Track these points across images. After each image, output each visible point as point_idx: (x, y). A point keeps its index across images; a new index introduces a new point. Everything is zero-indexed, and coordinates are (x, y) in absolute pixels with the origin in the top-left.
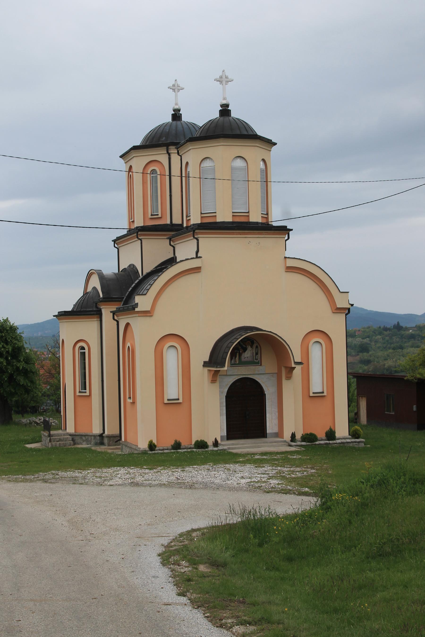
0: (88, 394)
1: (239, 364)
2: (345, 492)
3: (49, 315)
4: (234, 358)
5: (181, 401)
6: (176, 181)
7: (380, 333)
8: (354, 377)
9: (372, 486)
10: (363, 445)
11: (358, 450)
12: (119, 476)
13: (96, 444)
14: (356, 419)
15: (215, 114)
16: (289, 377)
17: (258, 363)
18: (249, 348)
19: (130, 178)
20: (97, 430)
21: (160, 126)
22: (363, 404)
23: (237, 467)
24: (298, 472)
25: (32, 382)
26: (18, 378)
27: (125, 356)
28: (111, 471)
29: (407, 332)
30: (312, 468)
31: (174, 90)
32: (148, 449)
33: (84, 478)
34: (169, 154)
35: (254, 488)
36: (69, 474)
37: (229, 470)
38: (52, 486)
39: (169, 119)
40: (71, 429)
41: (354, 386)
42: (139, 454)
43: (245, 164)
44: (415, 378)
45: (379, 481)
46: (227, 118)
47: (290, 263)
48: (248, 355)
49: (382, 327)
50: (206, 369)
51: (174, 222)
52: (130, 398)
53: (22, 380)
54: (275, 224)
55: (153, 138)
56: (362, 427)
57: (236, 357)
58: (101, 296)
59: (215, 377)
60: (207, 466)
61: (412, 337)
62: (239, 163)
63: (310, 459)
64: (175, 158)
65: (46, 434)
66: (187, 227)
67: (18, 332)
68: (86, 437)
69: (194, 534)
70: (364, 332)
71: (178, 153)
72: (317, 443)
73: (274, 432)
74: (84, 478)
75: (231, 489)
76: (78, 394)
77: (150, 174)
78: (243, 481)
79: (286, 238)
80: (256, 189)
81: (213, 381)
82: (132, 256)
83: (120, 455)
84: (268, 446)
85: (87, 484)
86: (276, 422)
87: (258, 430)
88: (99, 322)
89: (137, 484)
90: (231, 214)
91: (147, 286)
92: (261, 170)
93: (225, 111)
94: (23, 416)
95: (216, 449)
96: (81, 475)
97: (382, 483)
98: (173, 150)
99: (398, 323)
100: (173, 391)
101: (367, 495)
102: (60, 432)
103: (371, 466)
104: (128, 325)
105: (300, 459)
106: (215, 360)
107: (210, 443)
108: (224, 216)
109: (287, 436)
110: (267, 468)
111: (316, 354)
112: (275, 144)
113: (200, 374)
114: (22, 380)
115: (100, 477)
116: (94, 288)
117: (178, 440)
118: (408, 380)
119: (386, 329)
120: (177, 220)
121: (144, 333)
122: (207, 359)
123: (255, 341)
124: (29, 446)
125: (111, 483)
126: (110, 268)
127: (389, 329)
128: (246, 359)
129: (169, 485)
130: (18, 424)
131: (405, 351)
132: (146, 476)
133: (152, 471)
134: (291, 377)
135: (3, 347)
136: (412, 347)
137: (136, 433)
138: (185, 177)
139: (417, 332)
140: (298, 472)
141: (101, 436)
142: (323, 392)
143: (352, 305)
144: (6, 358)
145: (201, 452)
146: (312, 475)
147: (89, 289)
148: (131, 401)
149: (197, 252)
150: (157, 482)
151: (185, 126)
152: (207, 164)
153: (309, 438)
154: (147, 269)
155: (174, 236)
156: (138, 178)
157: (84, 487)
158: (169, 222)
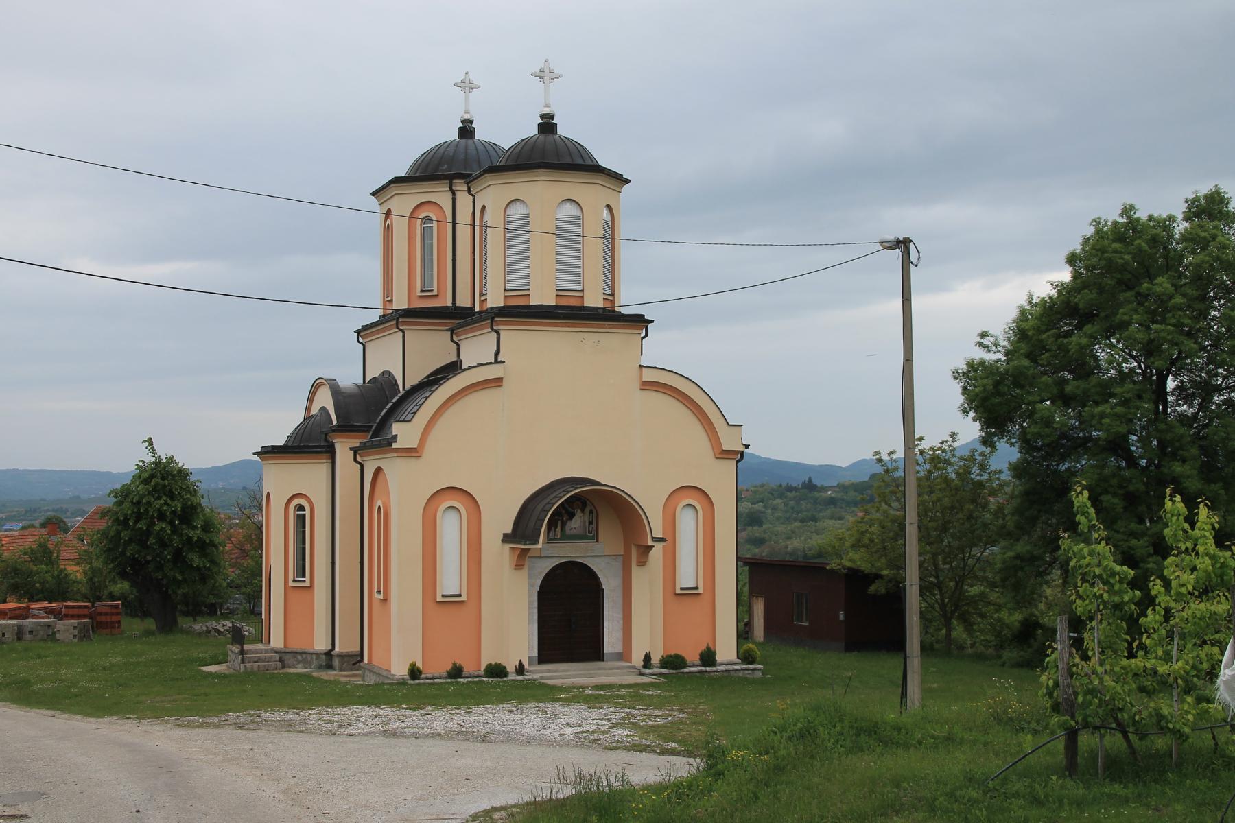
0: (308, 584)
2: (746, 748)
3: (246, 450)
5: (464, 598)
6: (463, 233)
7: (781, 496)
8: (746, 563)
9: (790, 739)
10: (759, 674)
11: (753, 682)
12: (363, 720)
13: (320, 667)
14: (747, 633)
15: (532, 130)
16: (642, 563)
17: (592, 538)
18: (579, 513)
19: (387, 228)
20: (321, 645)
21: (439, 147)
22: (759, 608)
23: (558, 708)
24: (659, 718)
25: (212, 562)
26: (190, 555)
27: (372, 522)
28: (349, 712)
29: (823, 495)
30: (680, 711)
31: (463, 89)
32: (407, 677)
33: (305, 722)
34: (454, 193)
35: (586, 741)
36: (278, 715)
37: (544, 712)
38: (250, 734)
39: (454, 136)
40: (277, 642)
41: (745, 578)
42: (392, 684)
43: (579, 213)
44: (844, 567)
45: (801, 730)
46: (550, 138)
47: (648, 376)
48: (576, 524)
49: (784, 485)
50: (507, 546)
51: (459, 303)
52: (379, 592)
53: (197, 561)
54: (624, 311)
55: (427, 166)
56: (758, 644)
58: (335, 422)
59: (521, 559)
60: (507, 706)
61: (832, 502)
62: (569, 210)
63: (675, 696)
64: (464, 200)
65: (236, 649)
66: (480, 312)
67: (192, 478)
68: (302, 656)
69: (497, 816)
70: (755, 492)
71: (469, 191)
72: (686, 670)
74: (305, 722)
75: (551, 743)
76: (291, 583)
78: (569, 731)
79: (643, 334)
80: (595, 250)
81: (519, 566)
82: (387, 357)
83: (361, 686)
84: (607, 675)
85: (310, 732)
86: (619, 635)
87: (591, 649)
88: (330, 465)
89: (394, 734)
90: (555, 293)
91: (411, 407)
92: (605, 223)
93: (547, 125)
94: (195, 620)
95: (520, 678)
96: (298, 718)
97: (807, 734)
98: (460, 186)
99: (810, 480)
100: (451, 581)
101: (783, 752)
102: (260, 646)
103: (787, 707)
104: (379, 470)
105: (659, 696)
106: (522, 531)
107: (511, 668)
108: (542, 296)
109: (637, 659)
110: (607, 710)
111: (688, 524)
112: (628, 181)
113: (496, 554)
114: (197, 561)
115: (332, 722)
116: (323, 409)
117: (458, 662)
118: (832, 571)
119: (790, 489)
120: (463, 301)
121: (405, 485)
122: (509, 531)
124: (206, 669)
125: (349, 731)
126: (350, 377)
127: (796, 489)
128: (573, 532)
129: (447, 735)
130: (188, 632)
131: (820, 524)
132: (408, 721)
133: (417, 713)
135: (166, 503)
136: (831, 518)
137: (388, 650)
138: (478, 226)
139: (839, 495)
140: (659, 718)
141: (328, 654)
142: (697, 588)
143: (747, 446)
144: (171, 523)
145: (495, 684)
146: (681, 722)
147: (314, 411)
148: (381, 597)
149: (497, 354)
150: (426, 731)
151: (480, 147)
152: (517, 210)
153: (673, 662)
154: (413, 380)
155: (459, 326)
156: (400, 226)
157: (306, 737)
158: (450, 304)
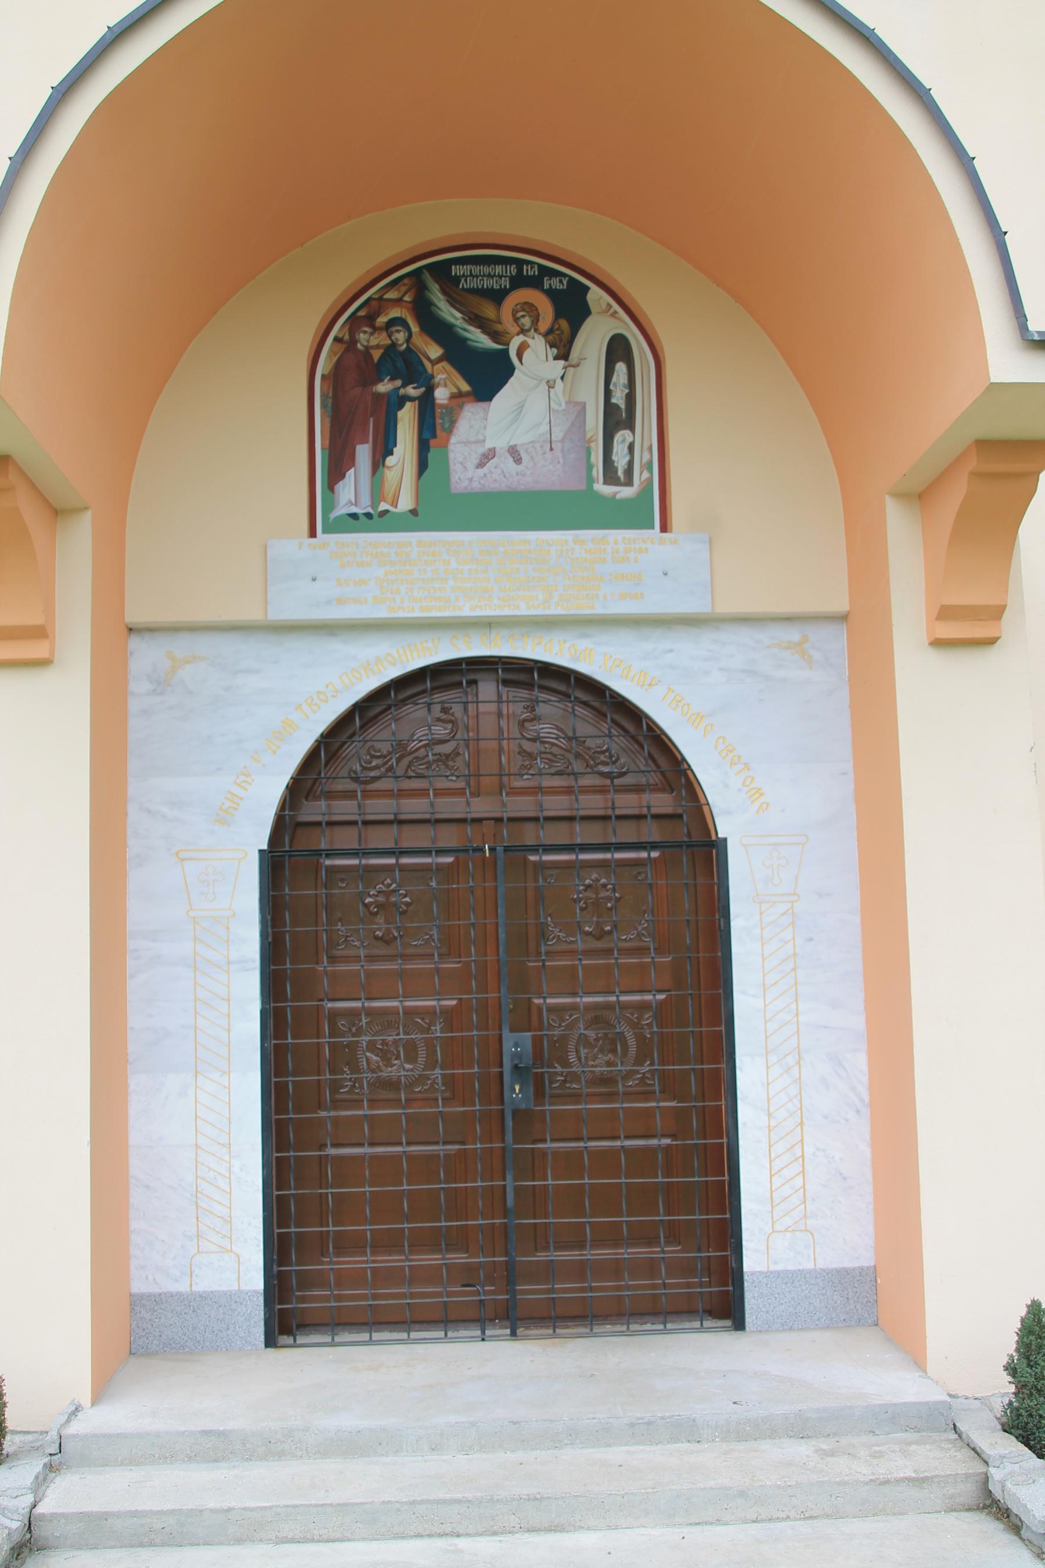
1: (416, 519)
4: (363, 453)
18: (534, 360)
57: (384, 448)
73: (829, 1258)
77: (545, 998)
86: (845, 1146)
123: (596, 296)
128: (502, 475)
134: (997, 612)
